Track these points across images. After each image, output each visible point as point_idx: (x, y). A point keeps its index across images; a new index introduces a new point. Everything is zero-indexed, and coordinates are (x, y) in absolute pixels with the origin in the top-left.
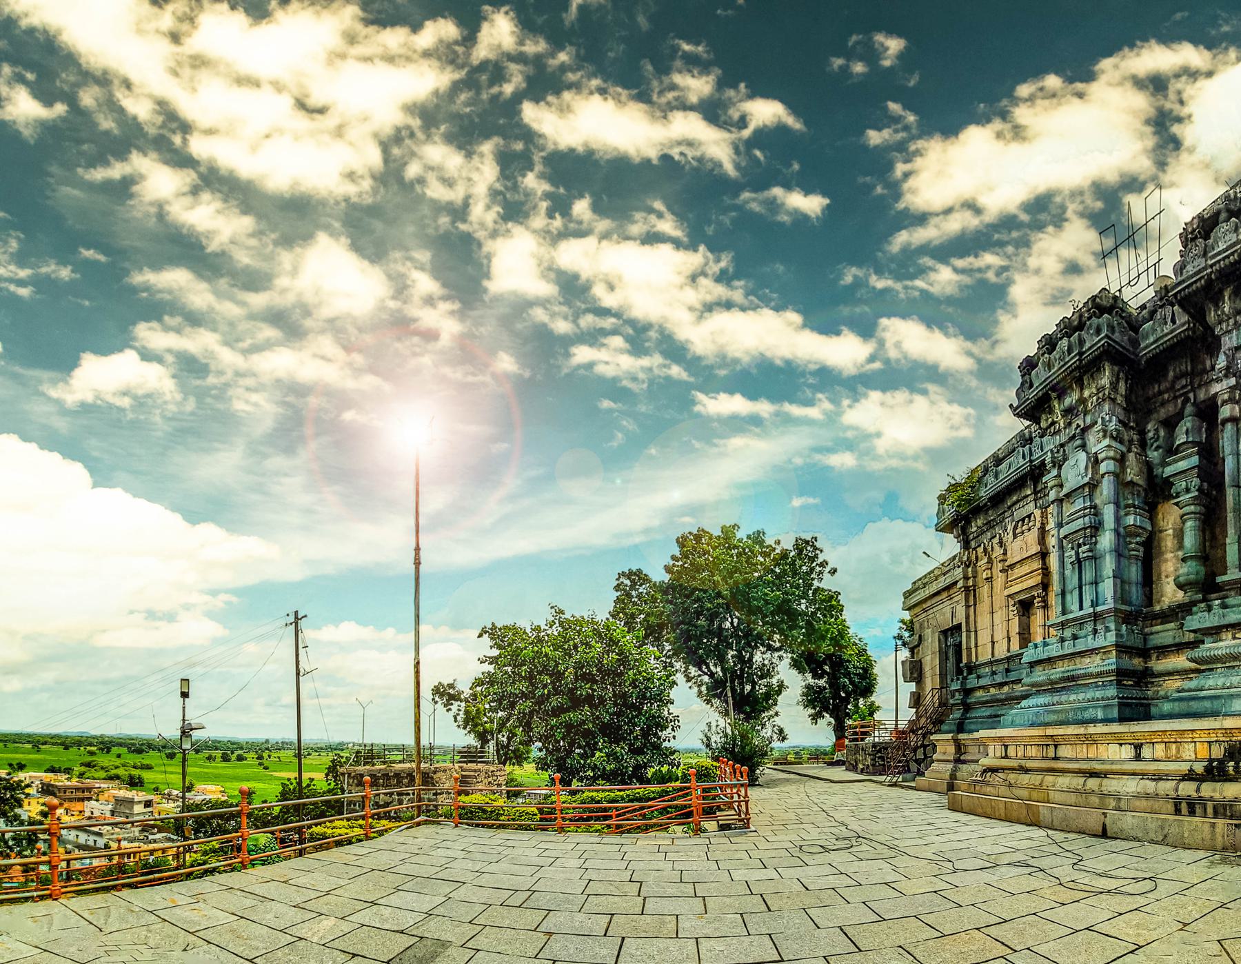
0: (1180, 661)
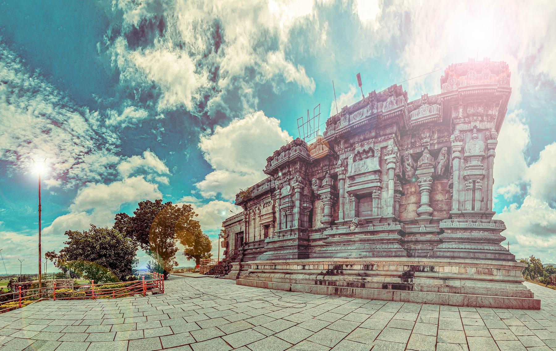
0: (321, 243)
